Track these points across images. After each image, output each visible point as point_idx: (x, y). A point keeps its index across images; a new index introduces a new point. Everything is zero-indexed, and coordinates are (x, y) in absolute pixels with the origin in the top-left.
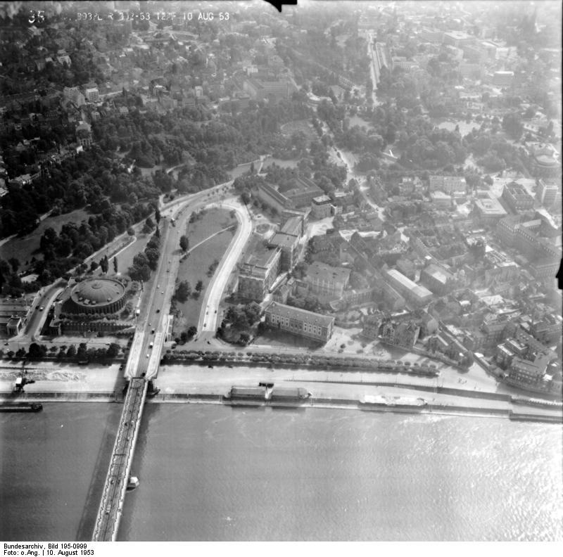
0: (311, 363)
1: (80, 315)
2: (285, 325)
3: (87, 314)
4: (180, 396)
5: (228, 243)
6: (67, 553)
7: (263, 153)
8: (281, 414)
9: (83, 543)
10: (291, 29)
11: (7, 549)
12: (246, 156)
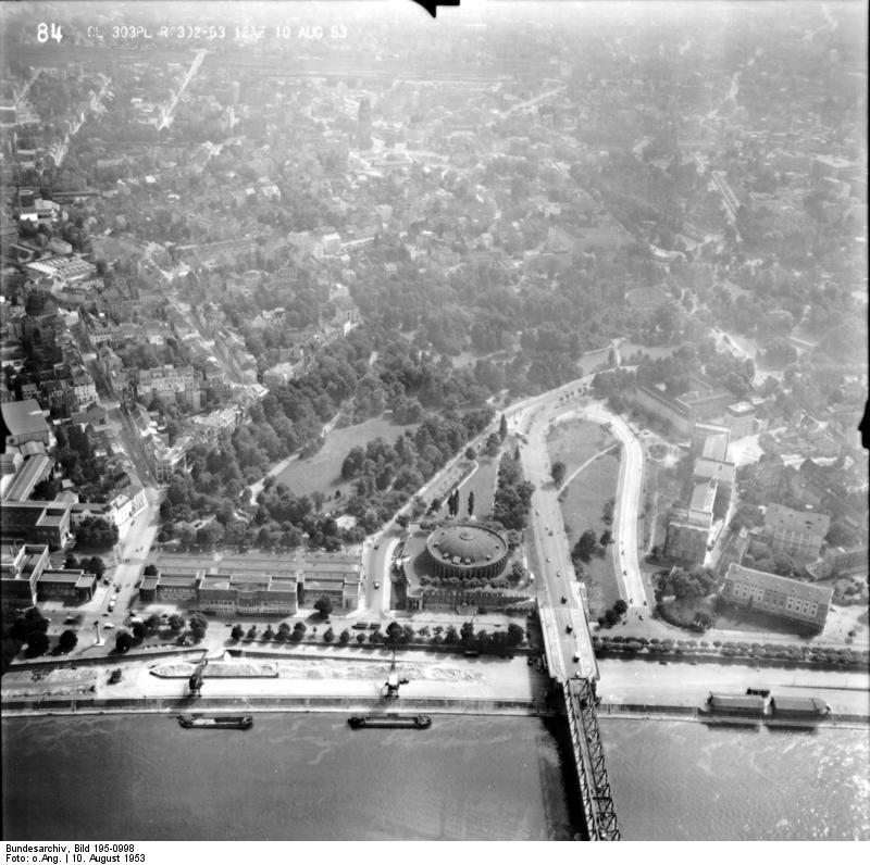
0: (814, 659)
1: (451, 579)
2: (811, 615)
3: (461, 579)
4: (633, 708)
5: (616, 472)
6: (104, 860)
7: (615, 336)
8: (782, 737)
9: (129, 843)
10: (583, 150)
11: (11, 853)
12: (592, 340)
